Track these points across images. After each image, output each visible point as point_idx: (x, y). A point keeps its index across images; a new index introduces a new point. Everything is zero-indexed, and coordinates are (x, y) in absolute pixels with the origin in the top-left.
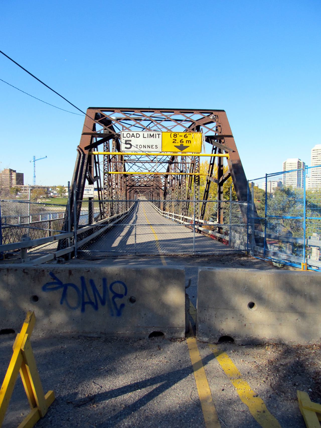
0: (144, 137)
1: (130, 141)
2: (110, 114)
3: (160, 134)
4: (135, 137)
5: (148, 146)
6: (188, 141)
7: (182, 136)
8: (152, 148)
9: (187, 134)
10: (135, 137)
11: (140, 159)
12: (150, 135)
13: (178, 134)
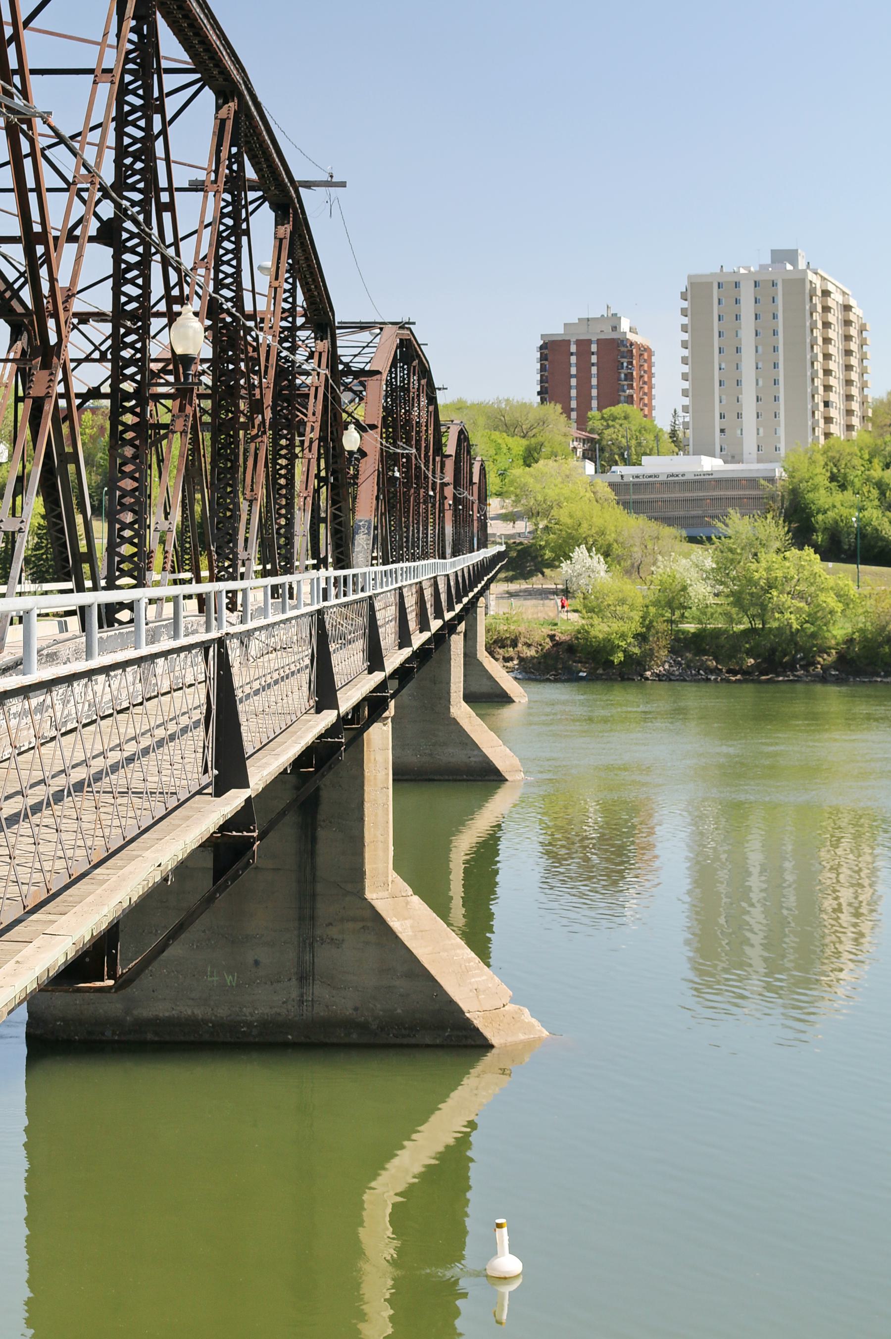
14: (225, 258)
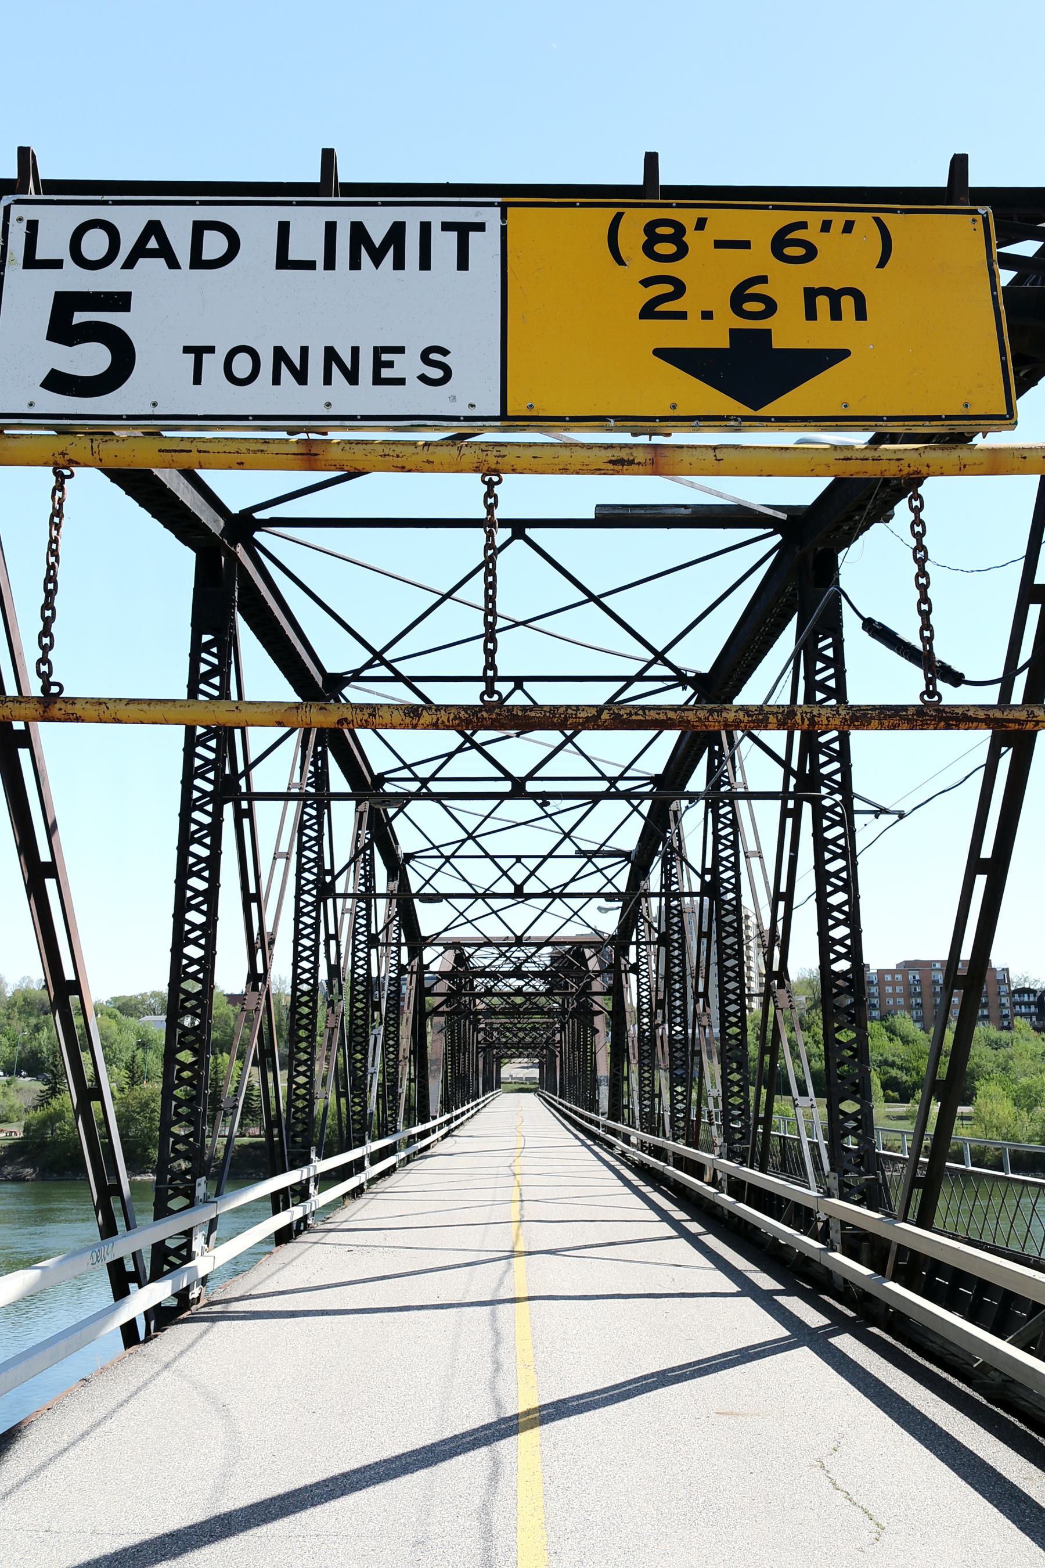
0: (283, 262)
1: (121, 301)
2: (319, 1238)
3: (480, 227)
4: (173, 263)
5: (331, 355)
6: (835, 296)
7: (745, 245)
8: (378, 380)
9: (803, 225)
10: (173, 263)
12: (358, 231)
13: (701, 224)
14: (305, 910)
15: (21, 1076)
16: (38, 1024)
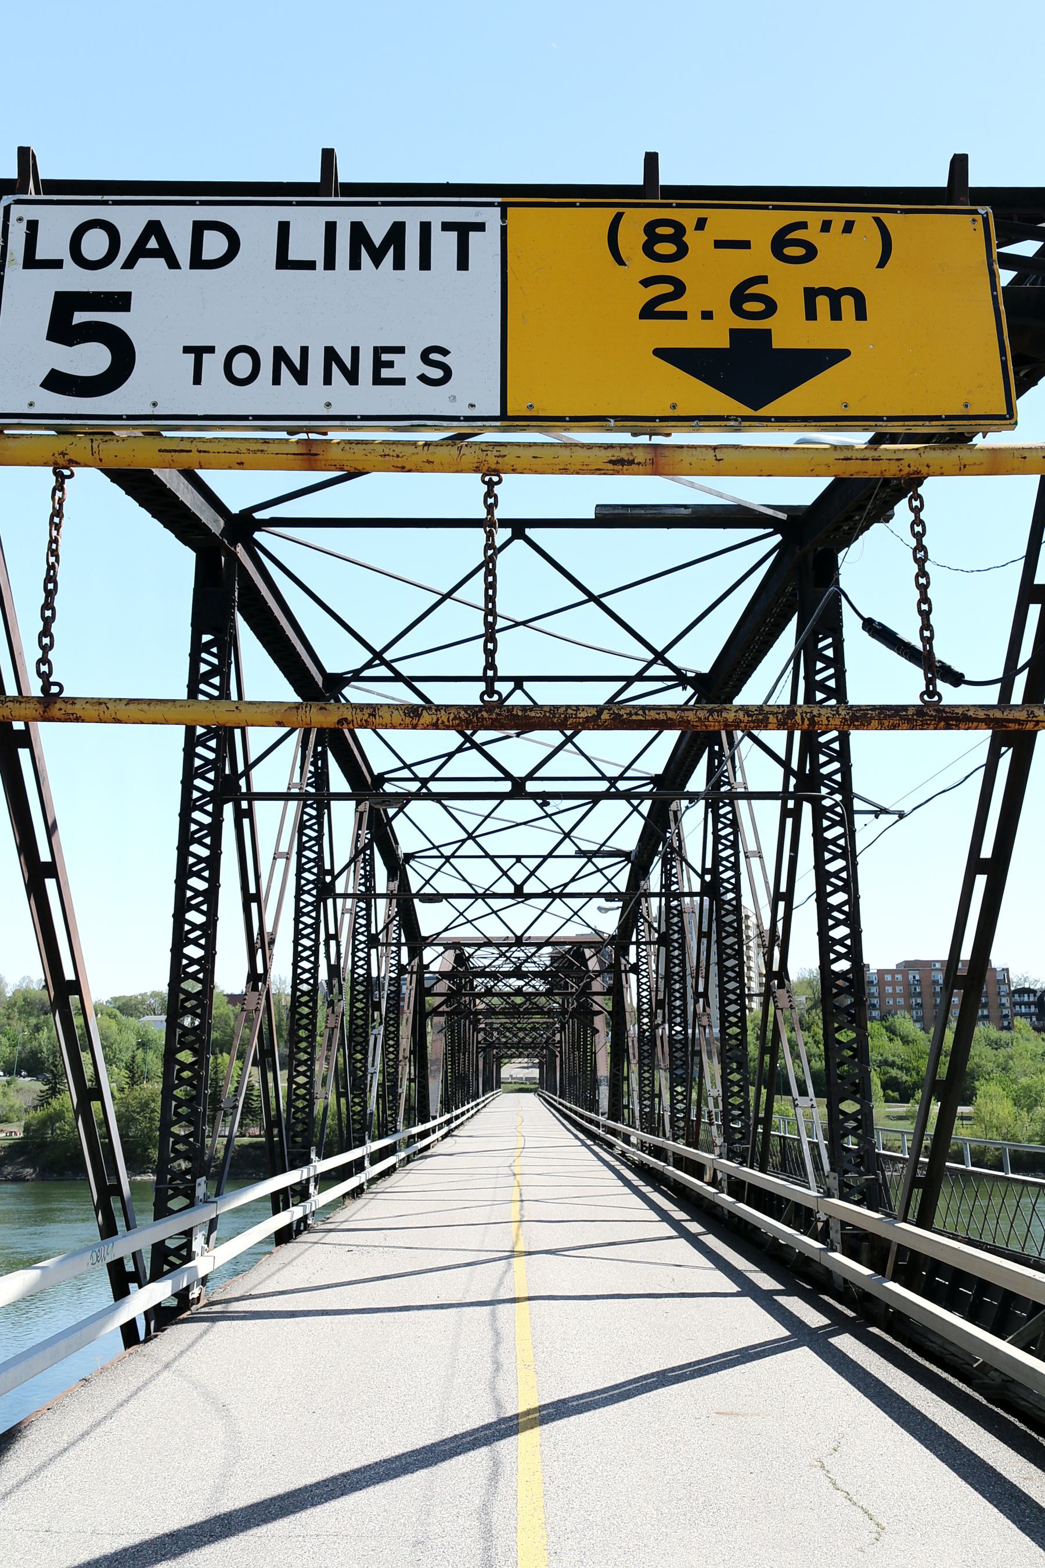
0: (283, 262)
1: (121, 301)
3: (480, 227)
4: (173, 263)
5: (331, 355)
6: (835, 296)
7: (745, 245)
8: (378, 380)
9: (803, 225)
10: (173, 263)
11: (451, 739)
12: (358, 231)
13: (701, 224)
14: (305, 910)
15: (21, 1076)
16: (38, 1024)
